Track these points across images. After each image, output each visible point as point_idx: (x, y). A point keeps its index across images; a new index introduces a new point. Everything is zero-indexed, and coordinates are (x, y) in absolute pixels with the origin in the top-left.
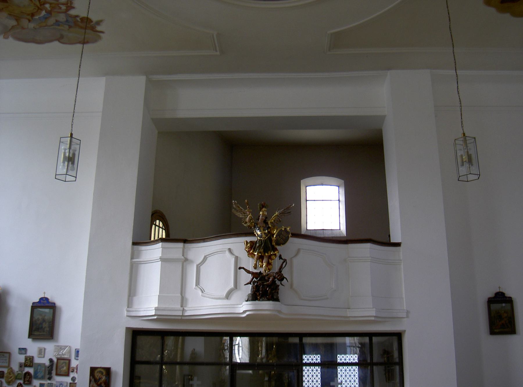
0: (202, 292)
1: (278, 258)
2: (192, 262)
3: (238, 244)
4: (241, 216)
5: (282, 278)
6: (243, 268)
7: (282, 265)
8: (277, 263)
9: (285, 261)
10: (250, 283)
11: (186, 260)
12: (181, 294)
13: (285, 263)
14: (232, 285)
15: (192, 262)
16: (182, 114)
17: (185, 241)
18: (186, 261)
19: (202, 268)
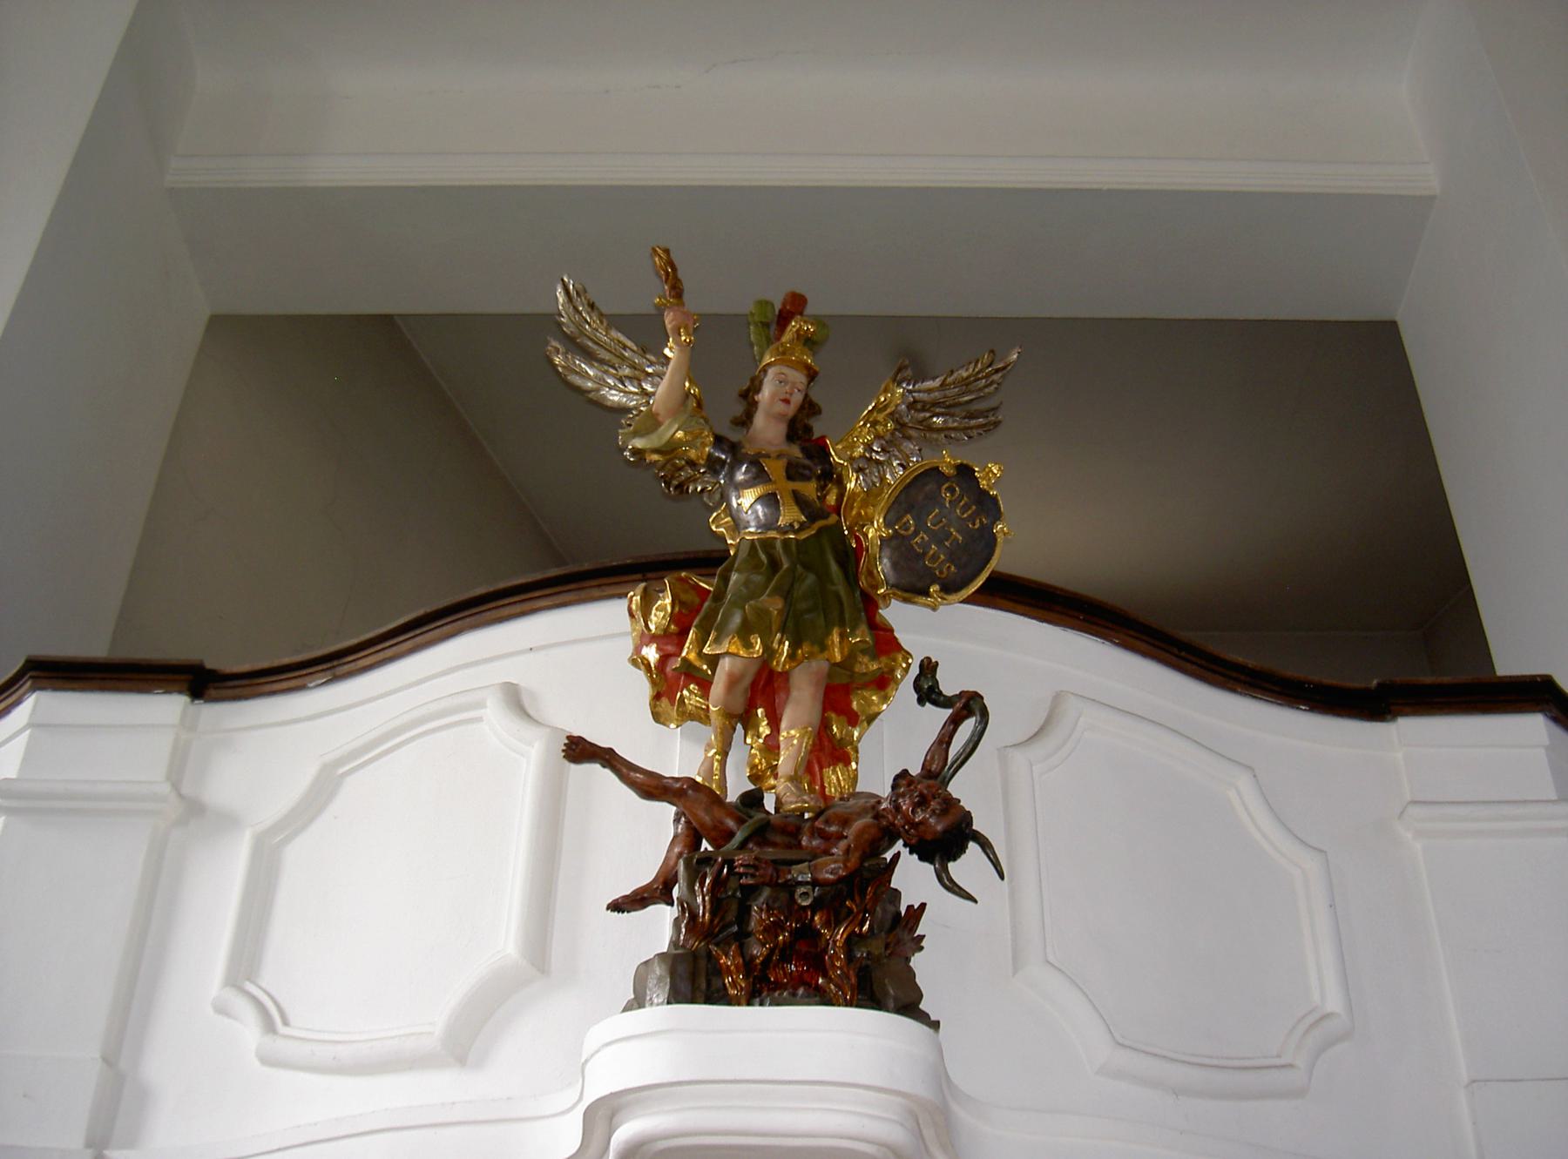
0: (269, 1027)
1: (905, 691)
2: (228, 822)
3: (585, 657)
4: (615, 397)
5: (947, 838)
6: (607, 758)
7: (945, 740)
8: (894, 740)
9: (969, 706)
10: (657, 892)
11: (194, 809)
12: (109, 1060)
13: (968, 727)
14: (505, 940)
15: (228, 822)
16: (339, 166)
17: (202, 683)
18: (194, 814)
19: (297, 855)
